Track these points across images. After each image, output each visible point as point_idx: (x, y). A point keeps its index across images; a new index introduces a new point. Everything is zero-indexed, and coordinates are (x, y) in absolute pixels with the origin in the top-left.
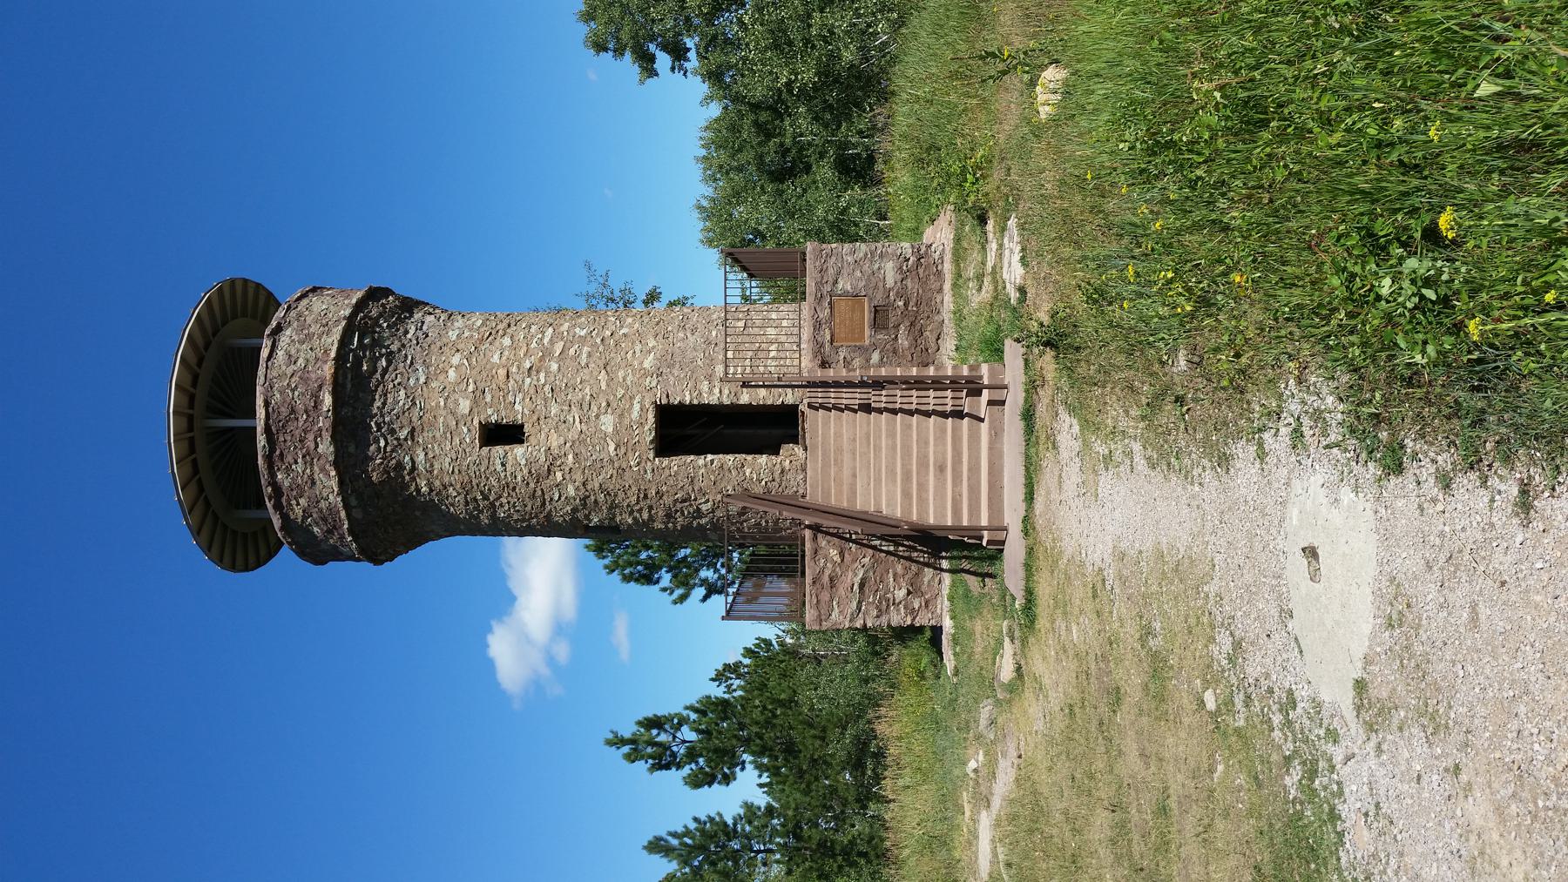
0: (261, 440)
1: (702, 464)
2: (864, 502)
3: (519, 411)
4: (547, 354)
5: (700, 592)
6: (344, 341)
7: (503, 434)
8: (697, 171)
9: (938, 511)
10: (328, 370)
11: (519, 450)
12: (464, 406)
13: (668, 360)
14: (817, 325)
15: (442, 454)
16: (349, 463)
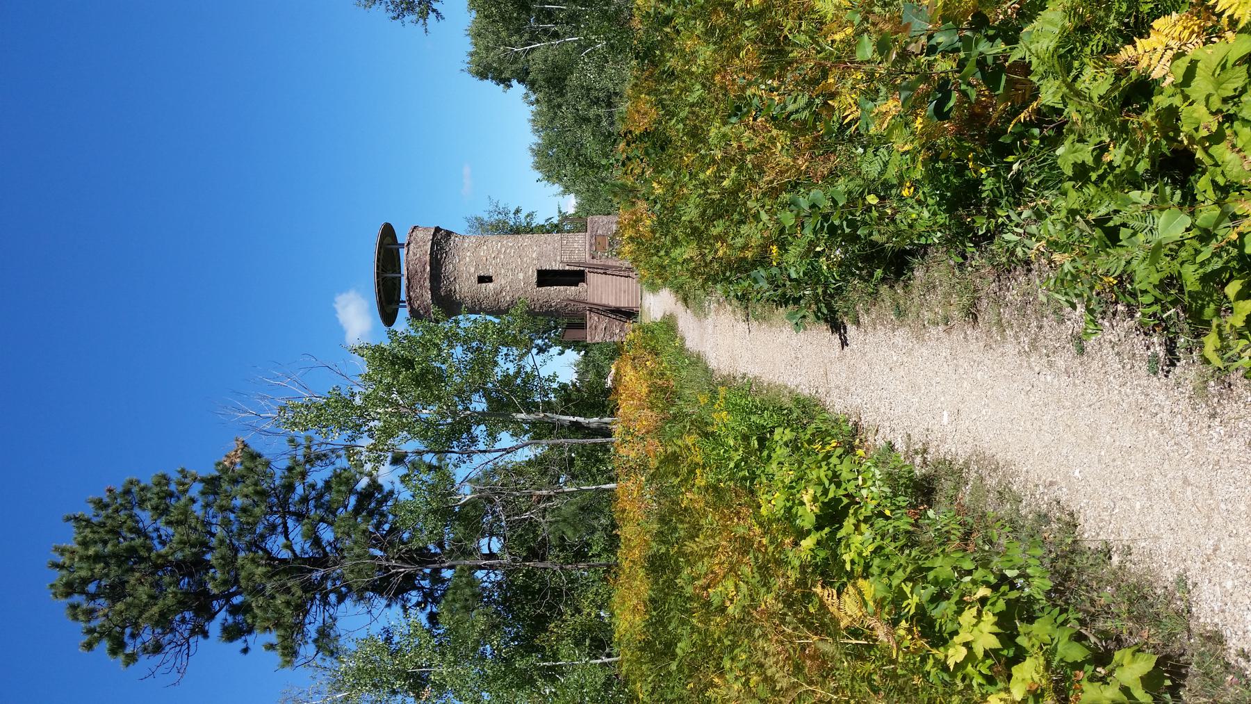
0: (404, 282)
1: (553, 290)
2: (604, 302)
3: (491, 272)
4: (499, 252)
5: (535, 351)
6: (432, 248)
7: (483, 279)
8: (529, 127)
9: (623, 303)
10: (428, 258)
11: (491, 285)
12: (472, 270)
13: (541, 255)
14: (591, 245)
15: (465, 286)
16: (435, 289)
